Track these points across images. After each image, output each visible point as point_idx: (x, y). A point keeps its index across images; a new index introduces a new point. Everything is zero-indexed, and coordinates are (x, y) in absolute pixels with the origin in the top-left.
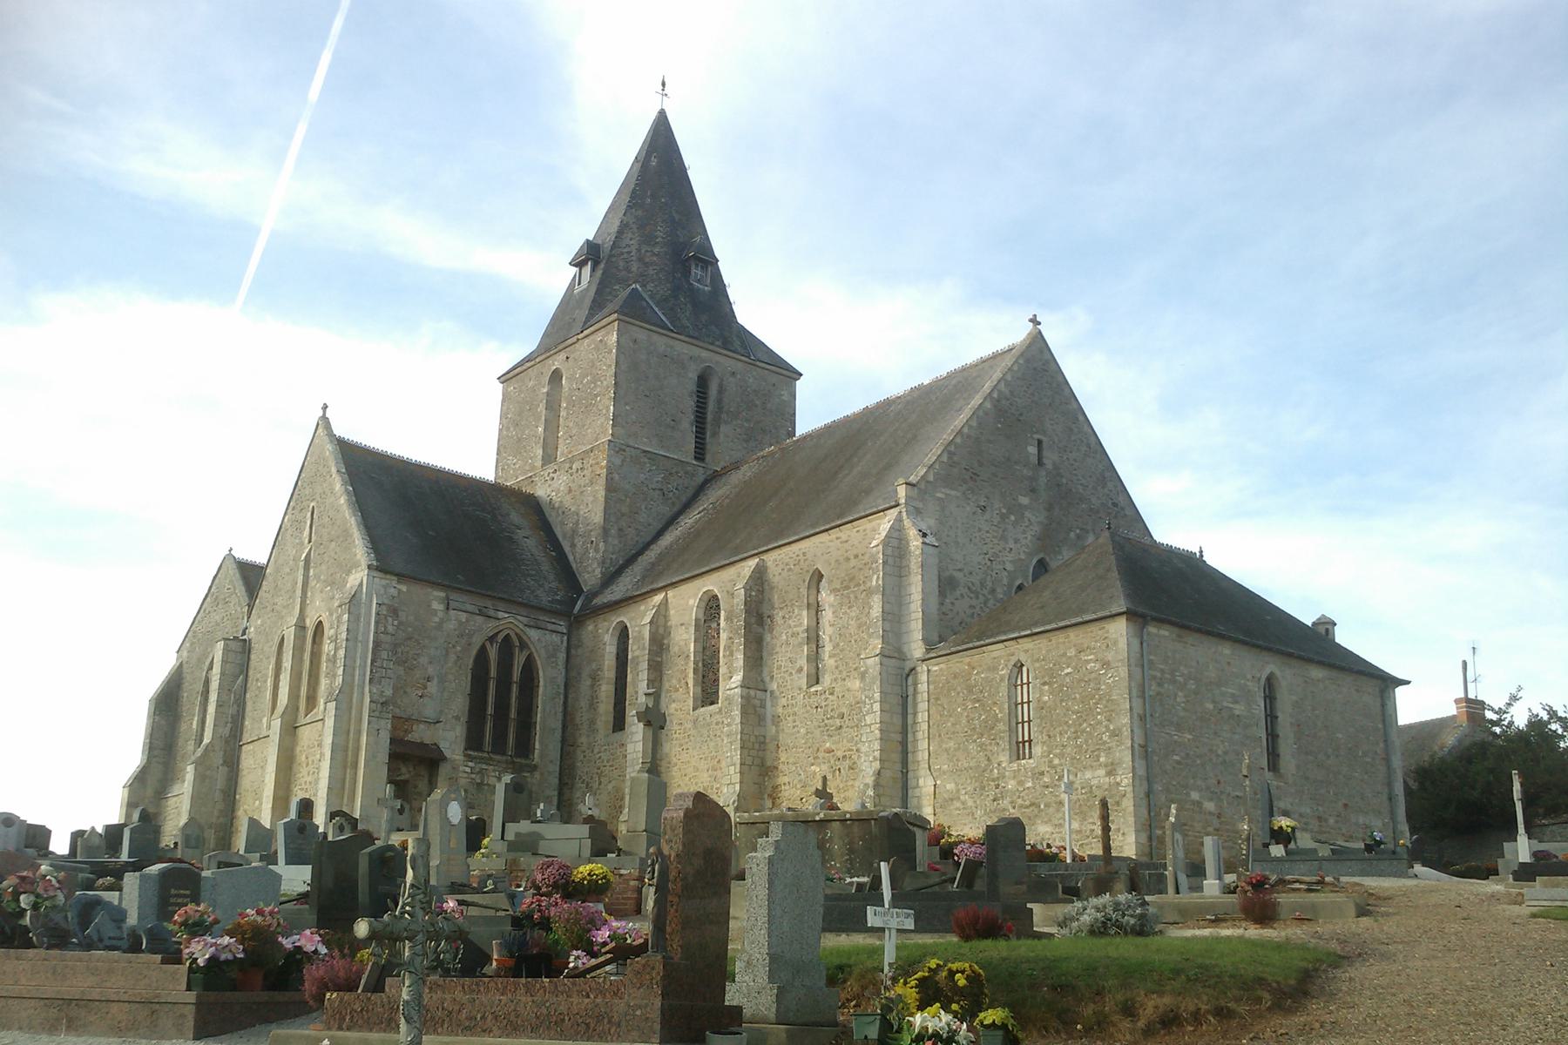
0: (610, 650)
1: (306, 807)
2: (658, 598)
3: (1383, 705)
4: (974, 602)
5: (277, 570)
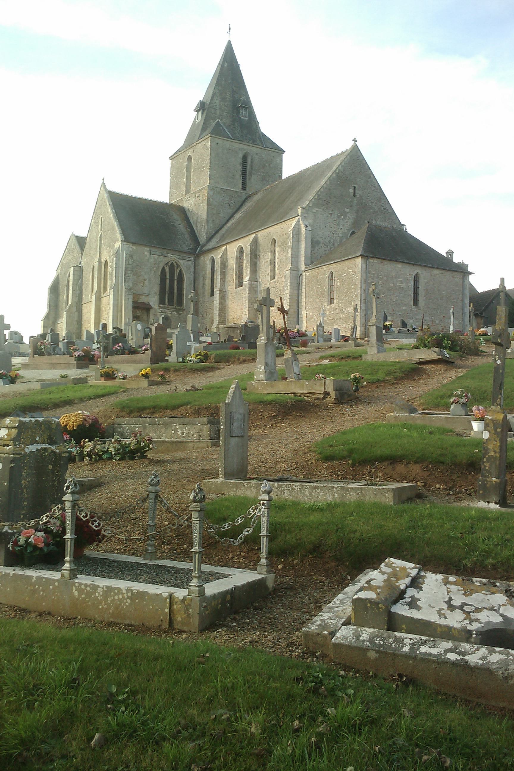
0: (209, 267)
1: (105, 326)
2: (224, 248)
3: (463, 282)
4: (326, 249)
5: (90, 241)
